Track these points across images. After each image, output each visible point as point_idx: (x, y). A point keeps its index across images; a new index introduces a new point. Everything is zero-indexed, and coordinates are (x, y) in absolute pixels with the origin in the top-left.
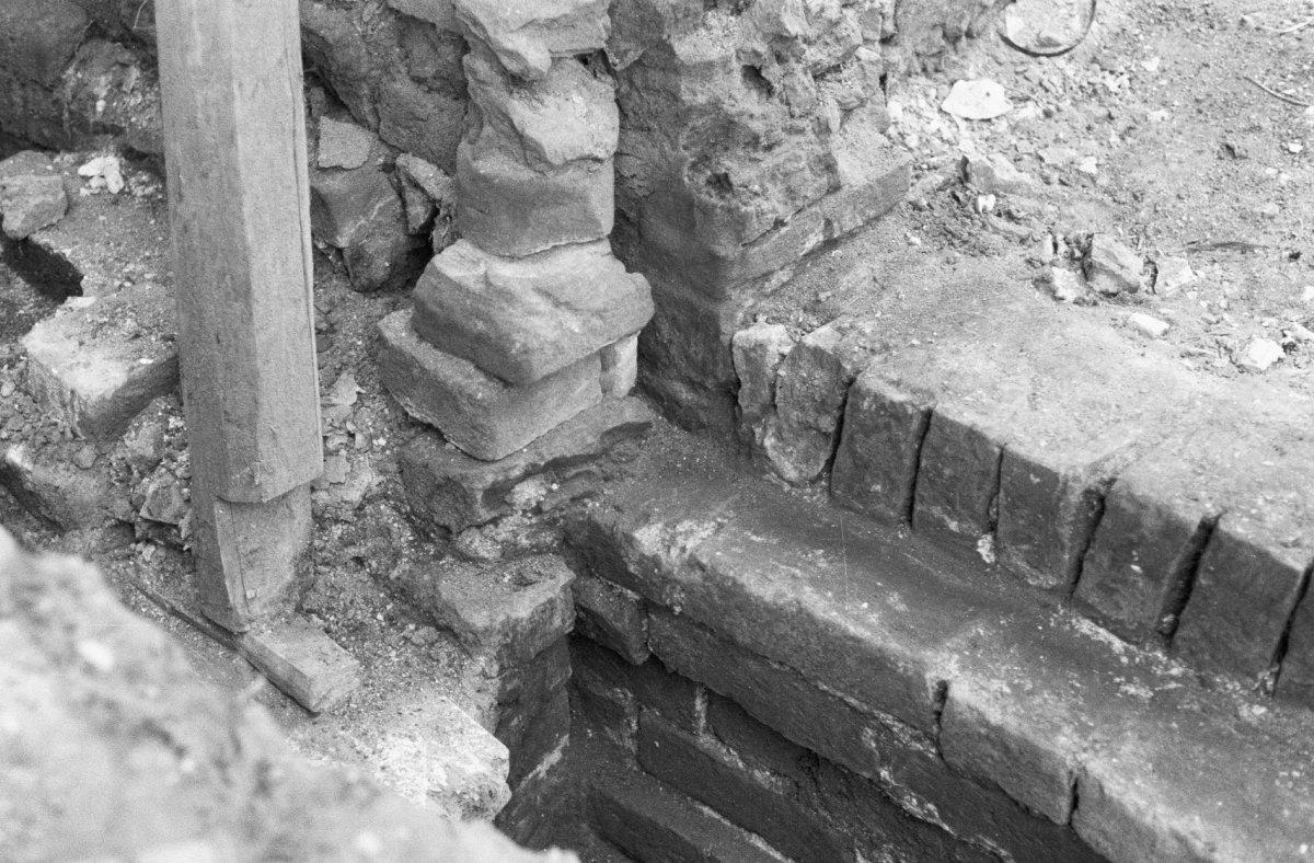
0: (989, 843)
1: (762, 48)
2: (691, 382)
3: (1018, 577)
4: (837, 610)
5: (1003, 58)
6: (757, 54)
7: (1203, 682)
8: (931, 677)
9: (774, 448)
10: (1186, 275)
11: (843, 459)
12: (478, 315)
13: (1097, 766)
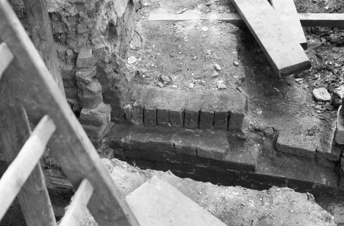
0: (185, 162)
1: (116, 67)
2: (120, 117)
3: (176, 127)
4: (155, 140)
5: (132, 52)
6: (115, 68)
7: (205, 131)
8: (172, 143)
9: (134, 122)
10: (175, 78)
11: (146, 120)
12: (92, 118)
13: (198, 146)
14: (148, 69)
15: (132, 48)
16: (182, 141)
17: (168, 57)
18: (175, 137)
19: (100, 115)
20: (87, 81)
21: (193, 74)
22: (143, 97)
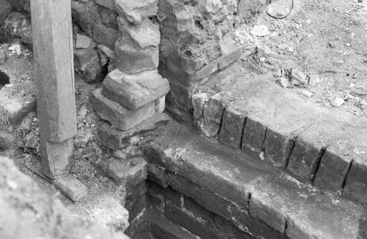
2: (180, 109)
3: (271, 164)
4: (220, 173)
5: (267, 19)
6: (199, 17)
7: (322, 193)
8: (246, 192)
9: (203, 127)
10: (318, 80)
11: (222, 131)
13: (292, 217)
14: (279, 54)
15: (269, 13)
16: (267, 195)
17: (324, 46)
18: (258, 182)
19: (136, 89)
20: (130, 17)
21: (352, 85)
22: (236, 89)
